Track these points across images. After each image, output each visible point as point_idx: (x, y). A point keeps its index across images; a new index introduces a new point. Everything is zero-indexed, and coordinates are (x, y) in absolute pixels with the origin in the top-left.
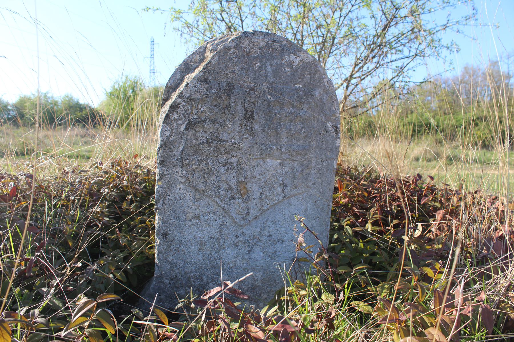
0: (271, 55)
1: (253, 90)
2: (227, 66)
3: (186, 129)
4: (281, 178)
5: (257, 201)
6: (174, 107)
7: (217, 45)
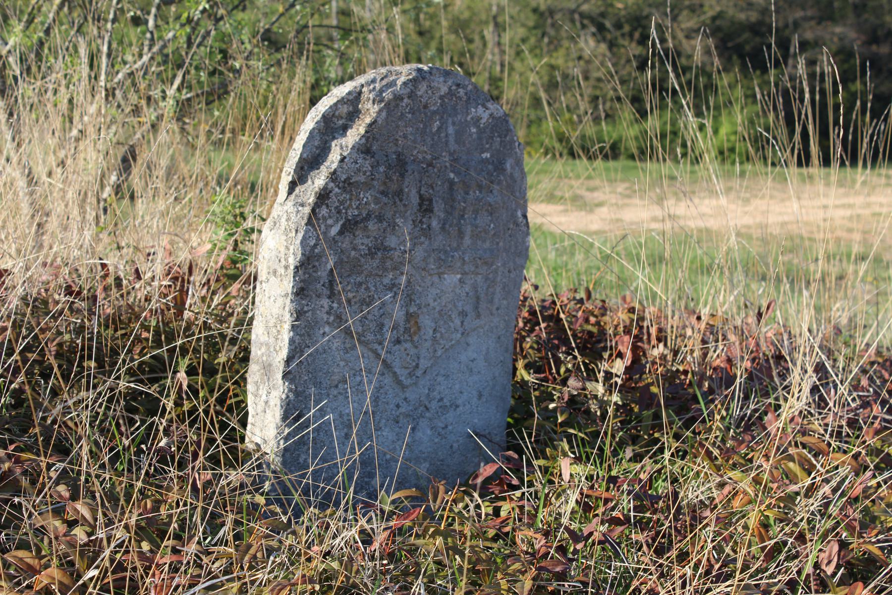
0: (454, 108)
1: (430, 165)
2: (398, 127)
3: (341, 233)
4: (460, 304)
5: (428, 344)
6: (323, 196)
7: (381, 91)
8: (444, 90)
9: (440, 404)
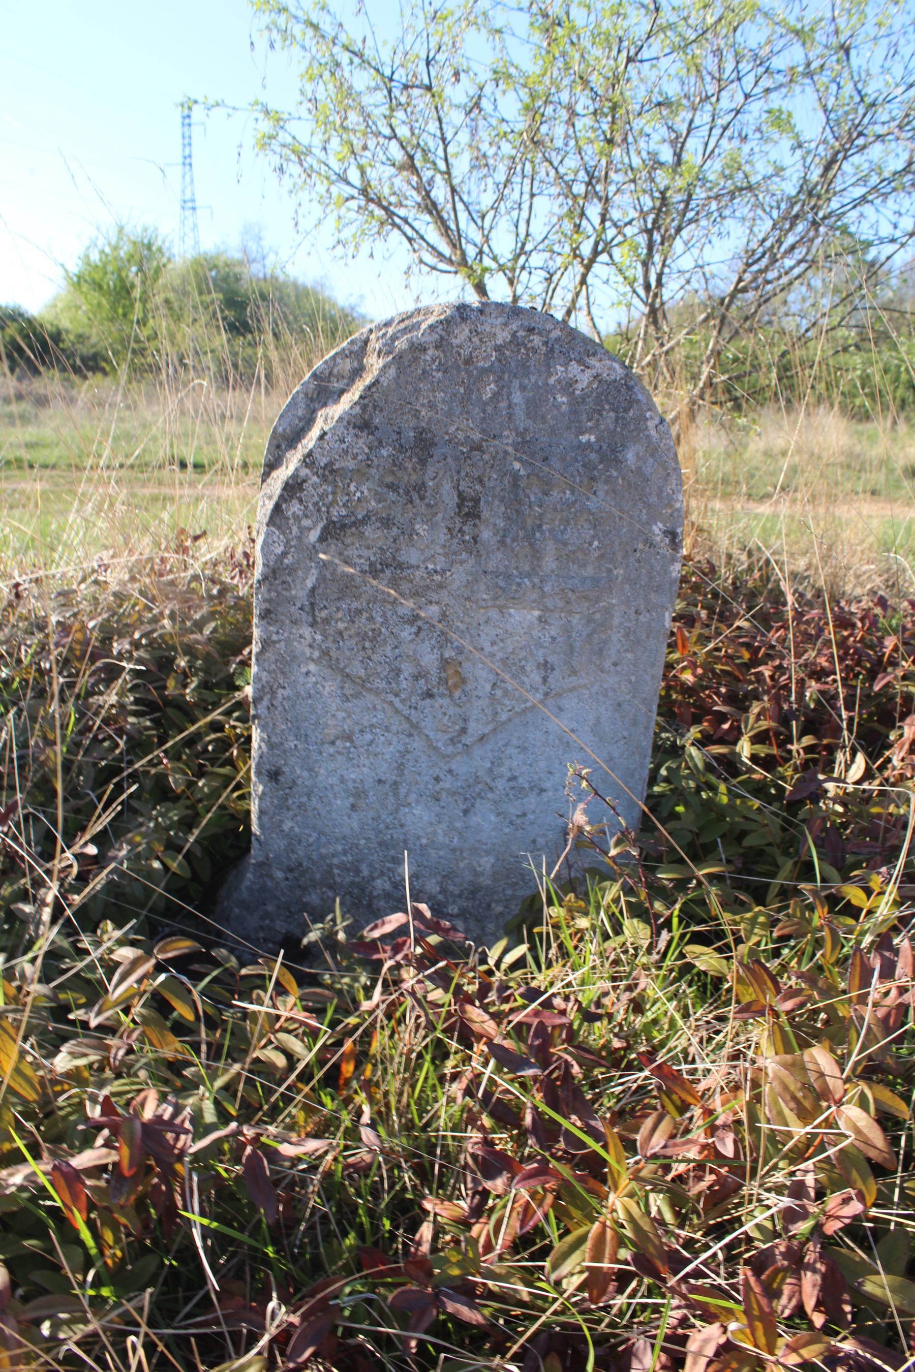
0: (524, 365)
1: (478, 448)
3: (322, 539)
6: (292, 488)
7: (394, 338)
8: (503, 336)
9: (512, 784)
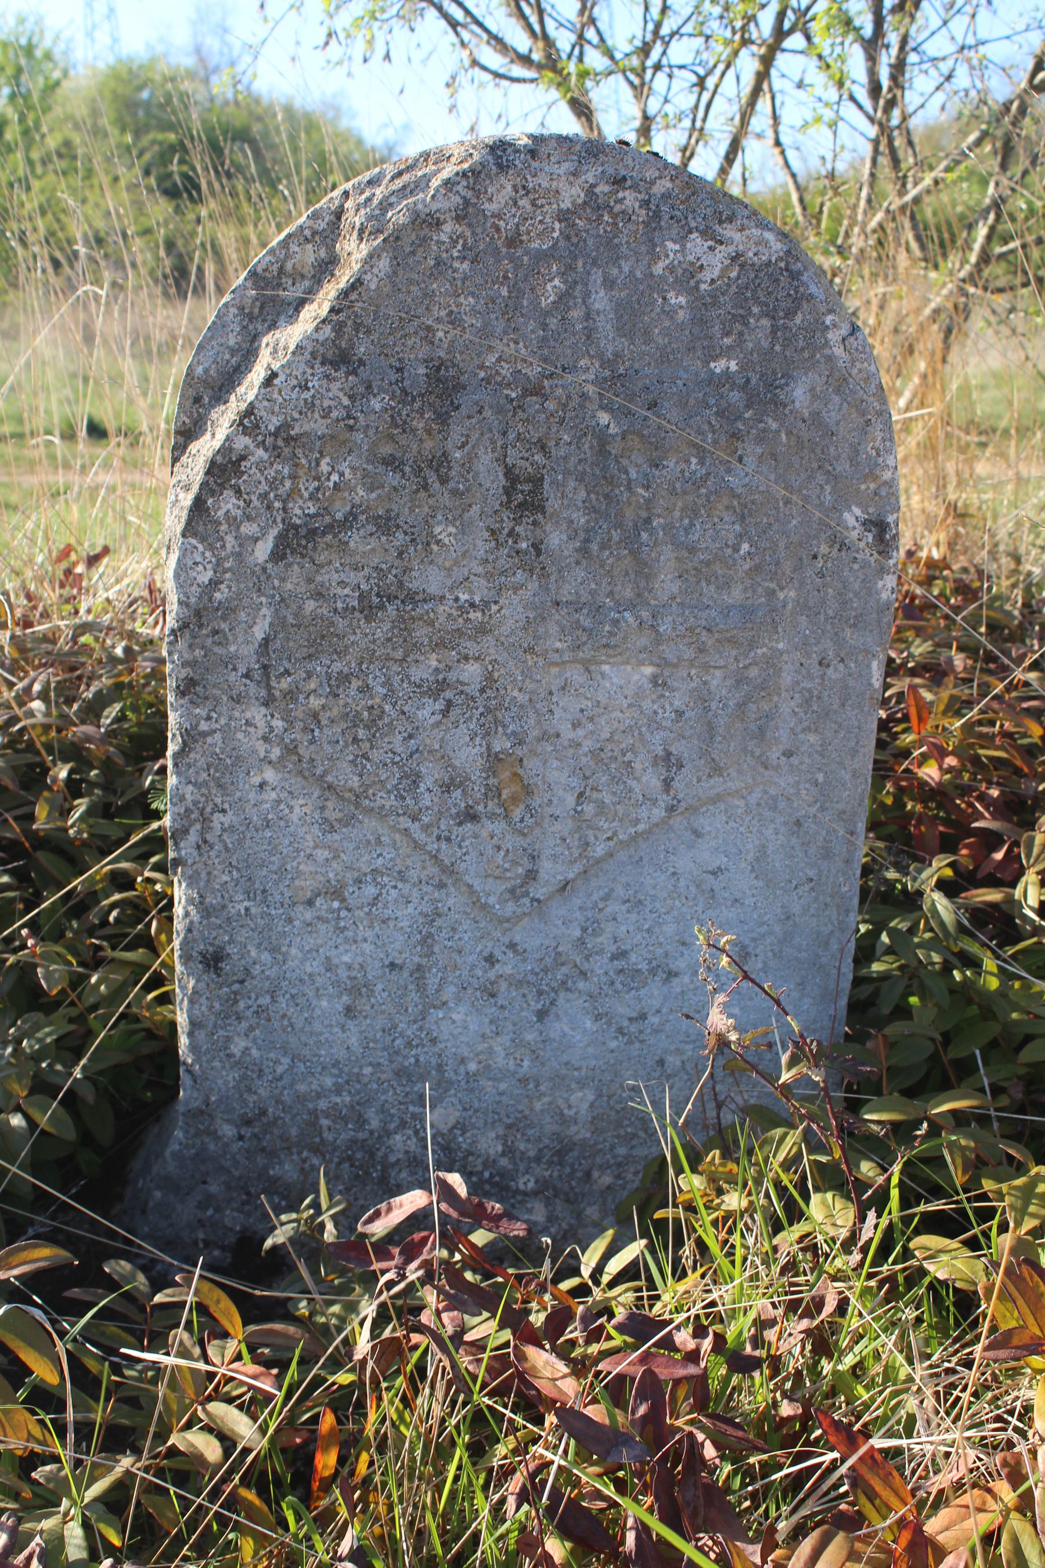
0: (609, 243)
1: (536, 390)
3: (277, 555)
5: (563, 827)
6: (223, 470)
7: (385, 205)
8: (571, 195)
